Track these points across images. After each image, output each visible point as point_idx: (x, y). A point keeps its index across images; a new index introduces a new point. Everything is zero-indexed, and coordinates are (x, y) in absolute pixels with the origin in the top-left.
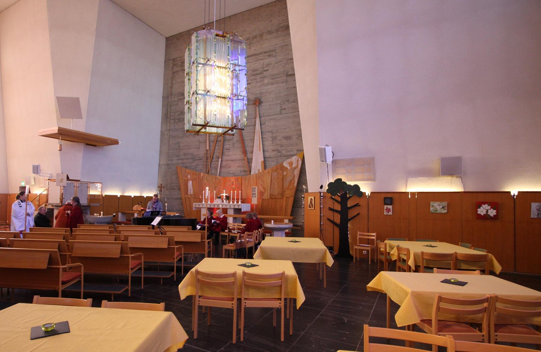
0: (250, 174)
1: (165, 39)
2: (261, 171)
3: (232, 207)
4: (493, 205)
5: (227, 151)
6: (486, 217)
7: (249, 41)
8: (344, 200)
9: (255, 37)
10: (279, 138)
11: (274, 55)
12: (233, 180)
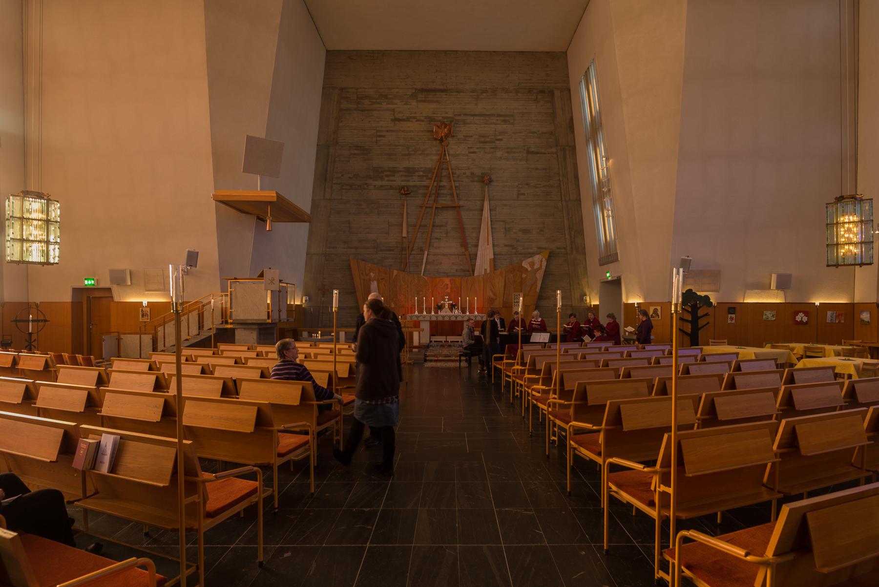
0: (473, 275)
1: (324, 54)
2: (488, 271)
3: (429, 319)
4: (806, 314)
5: (436, 240)
6: (801, 323)
7: (476, 94)
8: (695, 309)
9: (485, 91)
10: (514, 231)
11: (512, 121)
12: (447, 281)
